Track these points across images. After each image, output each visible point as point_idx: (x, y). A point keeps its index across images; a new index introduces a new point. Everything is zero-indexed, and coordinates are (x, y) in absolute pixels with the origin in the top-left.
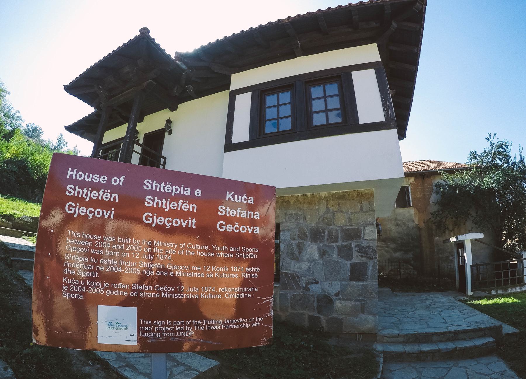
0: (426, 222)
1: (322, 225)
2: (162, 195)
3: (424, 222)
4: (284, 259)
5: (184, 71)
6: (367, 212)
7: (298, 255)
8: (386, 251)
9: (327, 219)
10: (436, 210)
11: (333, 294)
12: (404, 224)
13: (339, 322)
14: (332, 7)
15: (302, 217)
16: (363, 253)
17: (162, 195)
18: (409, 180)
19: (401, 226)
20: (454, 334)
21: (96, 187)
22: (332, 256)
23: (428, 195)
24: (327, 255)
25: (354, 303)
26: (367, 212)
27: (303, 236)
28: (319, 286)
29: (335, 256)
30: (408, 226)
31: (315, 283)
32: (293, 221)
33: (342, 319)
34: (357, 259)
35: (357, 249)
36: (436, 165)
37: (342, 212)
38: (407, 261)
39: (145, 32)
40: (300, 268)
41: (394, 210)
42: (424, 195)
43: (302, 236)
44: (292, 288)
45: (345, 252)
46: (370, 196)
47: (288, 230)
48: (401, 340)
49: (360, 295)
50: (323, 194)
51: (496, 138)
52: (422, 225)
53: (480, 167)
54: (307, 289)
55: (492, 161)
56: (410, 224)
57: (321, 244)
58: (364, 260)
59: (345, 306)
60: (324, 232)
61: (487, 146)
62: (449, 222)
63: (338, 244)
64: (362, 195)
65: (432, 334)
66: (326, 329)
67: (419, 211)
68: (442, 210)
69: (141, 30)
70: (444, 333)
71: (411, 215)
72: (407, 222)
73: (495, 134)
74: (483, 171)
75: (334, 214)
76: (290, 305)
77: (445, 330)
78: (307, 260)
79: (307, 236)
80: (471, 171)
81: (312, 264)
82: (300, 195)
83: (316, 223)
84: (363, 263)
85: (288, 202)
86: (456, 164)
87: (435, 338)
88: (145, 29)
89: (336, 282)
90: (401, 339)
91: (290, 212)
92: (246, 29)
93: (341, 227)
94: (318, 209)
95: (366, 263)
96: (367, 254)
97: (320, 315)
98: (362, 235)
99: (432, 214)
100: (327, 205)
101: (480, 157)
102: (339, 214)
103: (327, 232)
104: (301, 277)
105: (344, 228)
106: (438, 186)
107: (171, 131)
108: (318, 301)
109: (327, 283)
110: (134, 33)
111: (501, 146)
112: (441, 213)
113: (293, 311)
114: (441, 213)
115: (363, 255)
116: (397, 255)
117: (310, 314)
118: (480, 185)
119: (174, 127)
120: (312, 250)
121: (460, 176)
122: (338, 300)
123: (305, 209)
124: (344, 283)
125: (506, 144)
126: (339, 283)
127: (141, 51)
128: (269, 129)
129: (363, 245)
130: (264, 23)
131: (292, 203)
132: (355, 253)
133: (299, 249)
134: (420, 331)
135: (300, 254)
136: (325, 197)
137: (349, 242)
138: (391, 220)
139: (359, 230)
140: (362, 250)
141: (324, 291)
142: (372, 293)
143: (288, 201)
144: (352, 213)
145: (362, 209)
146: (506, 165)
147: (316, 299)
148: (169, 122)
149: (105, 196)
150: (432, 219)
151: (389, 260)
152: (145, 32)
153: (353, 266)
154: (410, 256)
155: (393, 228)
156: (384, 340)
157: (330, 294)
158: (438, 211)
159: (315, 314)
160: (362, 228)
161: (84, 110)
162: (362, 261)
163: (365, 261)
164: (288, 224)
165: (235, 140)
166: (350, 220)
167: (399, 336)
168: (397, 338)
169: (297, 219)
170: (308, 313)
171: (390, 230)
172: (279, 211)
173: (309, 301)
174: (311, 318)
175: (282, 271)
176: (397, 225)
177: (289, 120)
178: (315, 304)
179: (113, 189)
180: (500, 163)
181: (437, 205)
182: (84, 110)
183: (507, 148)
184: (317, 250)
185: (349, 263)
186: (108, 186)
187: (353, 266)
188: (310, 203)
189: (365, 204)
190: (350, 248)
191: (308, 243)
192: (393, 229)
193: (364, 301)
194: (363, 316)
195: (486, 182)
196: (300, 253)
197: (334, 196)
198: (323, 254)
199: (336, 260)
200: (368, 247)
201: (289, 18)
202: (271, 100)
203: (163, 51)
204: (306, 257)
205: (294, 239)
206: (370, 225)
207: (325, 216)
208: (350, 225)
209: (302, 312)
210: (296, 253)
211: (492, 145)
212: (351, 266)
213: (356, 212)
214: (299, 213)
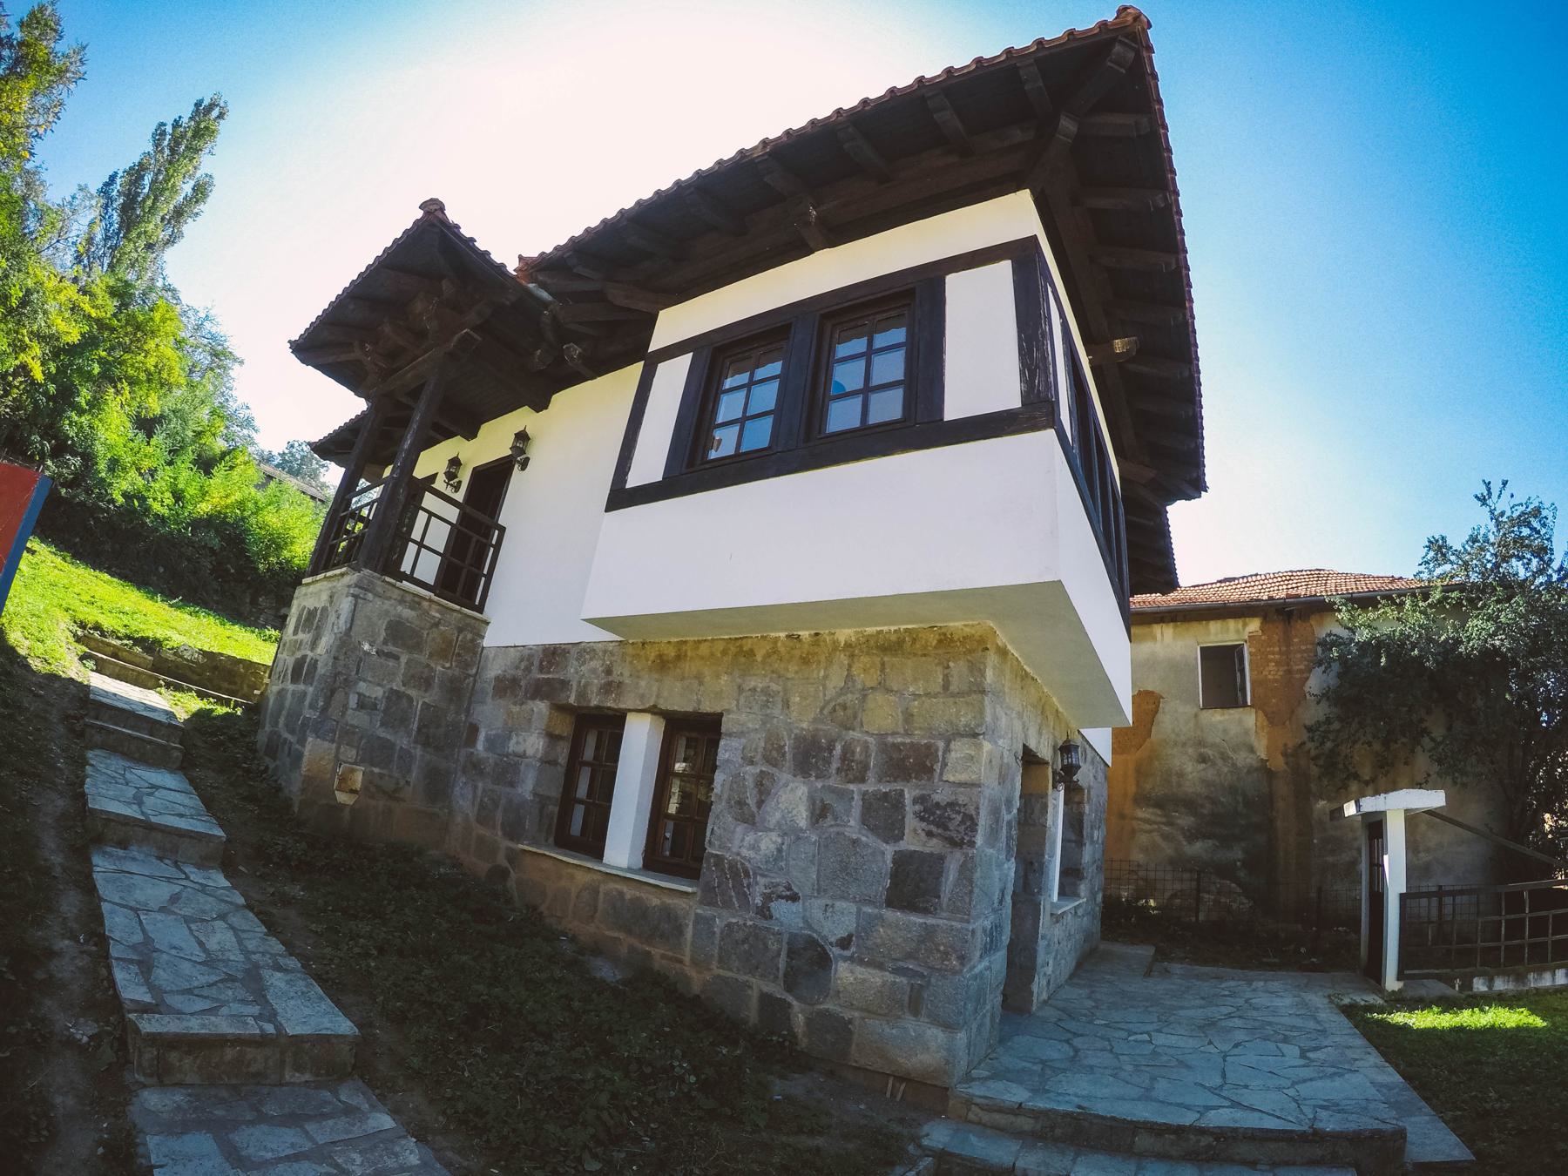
0: (1293, 755)
1: (831, 728)
3: (1285, 754)
4: (717, 817)
5: (545, 305)
6: (961, 694)
7: (754, 809)
8: (1166, 837)
9: (845, 708)
10: (1322, 718)
11: (833, 940)
12: (1224, 757)
13: (842, 1029)
14: (872, 96)
15: (779, 699)
16: (933, 822)
18: (1245, 625)
19: (1214, 764)
20: (1217, 1139)
23: (1300, 671)
24: (829, 820)
25: (890, 977)
26: (961, 694)
27: (774, 753)
28: (796, 907)
29: (852, 825)
30: (1234, 765)
31: (787, 898)
32: (756, 708)
33: (850, 1021)
34: (914, 839)
35: (918, 807)
36: (1331, 584)
37: (889, 691)
38: (1225, 871)
39: (433, 210)
40: (755, 847)
41: (1196, 715)
42: (1289, 672)
43: (773, 755)
44: (727, 904)
45: (884, 816)
46: (977, 646)
47: (742, 734)
48: (1027, 1127)
49: (910, 956)
50: (844, 634)
51: (1506, 494)
52: (1278, 763)
53: (1461, 587)
54: (764, 912)
55: (1497, 566)
56: (1243, 759)
57: (819, 785)
58: (934, 846)
59: (864, 980)
60: (830, 749)
61: (1481, 520)
62: (1362, 759)
63: (864, 787)
64: (952, 640)
65: (1136, 1127)
66: (804, 1043)
67: (1272, 719)
68: (1340, 719)
70: (1179, 1130)
71: (1246, 733)
72: (1234, 750)
73: (1505, 483)
74: (1464, 599)
75: (865, 696)
77: (1188, 1119)
78: (772, 829)
79: (784, 755)
80: (1426, 596)
81: (787, 840)
82: (782, 635)
83: (815, 720)
84: (932, 854)
85: (751, 653)
86: (1393, 580)
87: (1143, 1141)
88: (434, 201)
89: (844, 904)
90: (1026, 1123)
91: (756, 682)
92: (666, 185)
94: (826, 677)
96: (946, 829)
97: (790, 998)
98: (937, 767)
99: (1309, 729)
100: (850, 666)
101: (1457, 554)
102: (880, 697)
103: (838, 747)
104: (755, 874)
105: (890, 739)
106: (1326, 645)
107: (527, 460)
108: (792, 953)
109: (822, 902)
110: (408, 216)
111: (1523, 520)
112: (1336, 726)
113: (721, 972)
114: (1336, 726)
115: (934, 829)
116: (1198, 848)
117: (765, 989)
118: (1458, 642)
119: (535, 452)
120: (793, 798)
121: (1392, 613)
122: (845, 959)
123: (790, 675)
125: (1537, 512)
126: (853, 908)
127: (432, 254)
129: (937, 798)
130: (706, 164)
131: (759, 659)
132: (911, 822)
133: (760, 793)
134: (1102, 1109)
135: (759, 807)
136: (848, 645)
137: (898, 786)
138: (1184, 744)
139: (929, 751)
140: (934, 815)
141: (810, 927)
142: (946, 953)
143: (752, 650)
144: (916, 696)
145: (946, 686)
146: (1542, 579)
147: (785, 947)
148: (522, 437)
150: (1310, 745)
151: (1172, 861)
152: (433, 210)
153: (902, 860)
154: (1237, 853)
155: (1189, 767)
156: (971, 1116)
157: (825, 938)
158: (1328, 721)
159: (776, 990)
160: (941, 744)
161: (340, 405)
162: (927, 850)
163: (936, 851)
164: (743, 717)
165: (633, 481)
166: (908, 717)
167: (1019, 1110)
168: (1012, 1118)
169: (765, 705)
170: (762, 985)
171: (1181, 775)
172: (725, 677)
173: (766, 947)
174: (766, 999)
175: (709, 850)
176: (1203, 759)
177: (769, 420)
178: (782, 962)
180: (1522, 574)
181: (1324, 704)
182: (340, 405)
183: (1544, 525)
184: (805, 798)
185: (889, 850)
187: (902, 860)
188: (806, 661)
189: (958, 668)
190: (896, 802)
191: (784, 776)
192: (1191, 773)
193: (922, 976)
194: (911, 1025)
195: (1477, 630)
196: (760, 803)
197: (872, 643)
198: (820, 812)
199: (855, 836)
200: (952, 805)
201: (765, 142)
203: (485, 255)
204: (774, 818)
205: (752, 763)
206: (967, 736)
207: (840, 700)
208: (907, 734)
209: (746, 978)
210: (752, 802)
211: (1496, 518)
212: (894, 862)
213: (927, 695)
214: (774, 687)
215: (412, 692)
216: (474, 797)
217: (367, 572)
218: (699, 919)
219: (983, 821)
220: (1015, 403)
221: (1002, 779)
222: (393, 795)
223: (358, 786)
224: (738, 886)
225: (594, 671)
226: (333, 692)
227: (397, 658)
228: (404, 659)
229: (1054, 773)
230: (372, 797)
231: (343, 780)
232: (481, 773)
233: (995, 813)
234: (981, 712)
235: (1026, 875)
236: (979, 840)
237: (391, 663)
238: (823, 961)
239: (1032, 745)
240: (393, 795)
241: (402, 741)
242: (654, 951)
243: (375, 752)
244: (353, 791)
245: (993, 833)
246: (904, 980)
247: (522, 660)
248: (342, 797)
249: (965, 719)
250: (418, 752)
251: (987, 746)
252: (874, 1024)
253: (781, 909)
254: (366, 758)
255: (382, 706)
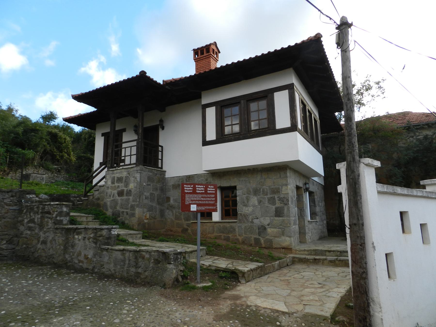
2: (199, 188)
17: (199, 188)
21: (189, 187)
22: (265, 203)
24: (262, 203)
28: (258, 220)
29: (267, 204)
34: (278, 204)
44: (244, 222)
47: (241, 189)
49: (281, 225)
54: (252, 222)
69: (140, 73)
76: (243, 232)
93: (269, 187)
95: (283, 207)
97: (260, 237)
108: (259, 229)
109: (263, 218)
120: (254, 200)
124: (272, 218)
126: (269, 218)
128: (227, 130)
129: (281, 197)
132: (277, 201)
140: (281, 200)
149: (191, 189)
153: (276, 209)
159: (257, 237)
168: (304, 252)
170: (254, 236)
174: (256, 239)
175: (238, 213)
178: (257, 231)
179: (192, 187)
185: (274, 207)
186: (191, 187)
190: (274, 198)
191: (252, 196)
194: (283, 238)
196: (248, 202)
198: (260, 202)
202: (227, 112)
205: (244, 194)
208: (274, 186)
210: (246, 202)
215: (154, 192)
216: (173, 214)
217: (141, 166)
218: (239, 227)
219: (290, 200)
220: (289, 125)
221: (292, 192)
222: (155, 218)
223: (148, 217)
224: (246, 219)
225: (202, 180)
226: (140, 196)
227: (150, 185)
228: (152, 185)
229: (304, 189)
230: (151, 219)
231: (145, 216)
232: (174, 208)
233: (292, 198)
234: (287, 181)
235: (301, 213)
236: (290, 203)
237: (149, 186)
238: (265, 229)
239: (298, 184)
240: (155, 218)
241: (154, 205)
242: (229, 235)
243: (151, 209)
244: (147, 219)
245: (292, 202)
246: (280, 230)
247: (180, 180)
248: (146, 221)
249: (284, 182)
250: (158, 206)
251: (289, 187)
252: (277, 239)
253: (255, 221)
254: (149, 210)
255: (149, 197)
